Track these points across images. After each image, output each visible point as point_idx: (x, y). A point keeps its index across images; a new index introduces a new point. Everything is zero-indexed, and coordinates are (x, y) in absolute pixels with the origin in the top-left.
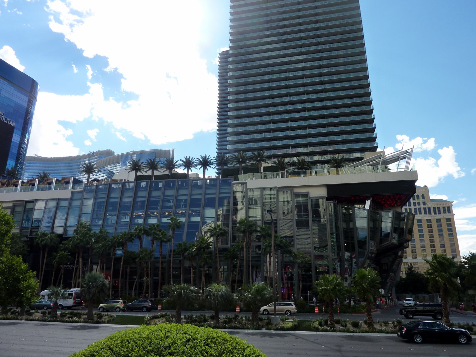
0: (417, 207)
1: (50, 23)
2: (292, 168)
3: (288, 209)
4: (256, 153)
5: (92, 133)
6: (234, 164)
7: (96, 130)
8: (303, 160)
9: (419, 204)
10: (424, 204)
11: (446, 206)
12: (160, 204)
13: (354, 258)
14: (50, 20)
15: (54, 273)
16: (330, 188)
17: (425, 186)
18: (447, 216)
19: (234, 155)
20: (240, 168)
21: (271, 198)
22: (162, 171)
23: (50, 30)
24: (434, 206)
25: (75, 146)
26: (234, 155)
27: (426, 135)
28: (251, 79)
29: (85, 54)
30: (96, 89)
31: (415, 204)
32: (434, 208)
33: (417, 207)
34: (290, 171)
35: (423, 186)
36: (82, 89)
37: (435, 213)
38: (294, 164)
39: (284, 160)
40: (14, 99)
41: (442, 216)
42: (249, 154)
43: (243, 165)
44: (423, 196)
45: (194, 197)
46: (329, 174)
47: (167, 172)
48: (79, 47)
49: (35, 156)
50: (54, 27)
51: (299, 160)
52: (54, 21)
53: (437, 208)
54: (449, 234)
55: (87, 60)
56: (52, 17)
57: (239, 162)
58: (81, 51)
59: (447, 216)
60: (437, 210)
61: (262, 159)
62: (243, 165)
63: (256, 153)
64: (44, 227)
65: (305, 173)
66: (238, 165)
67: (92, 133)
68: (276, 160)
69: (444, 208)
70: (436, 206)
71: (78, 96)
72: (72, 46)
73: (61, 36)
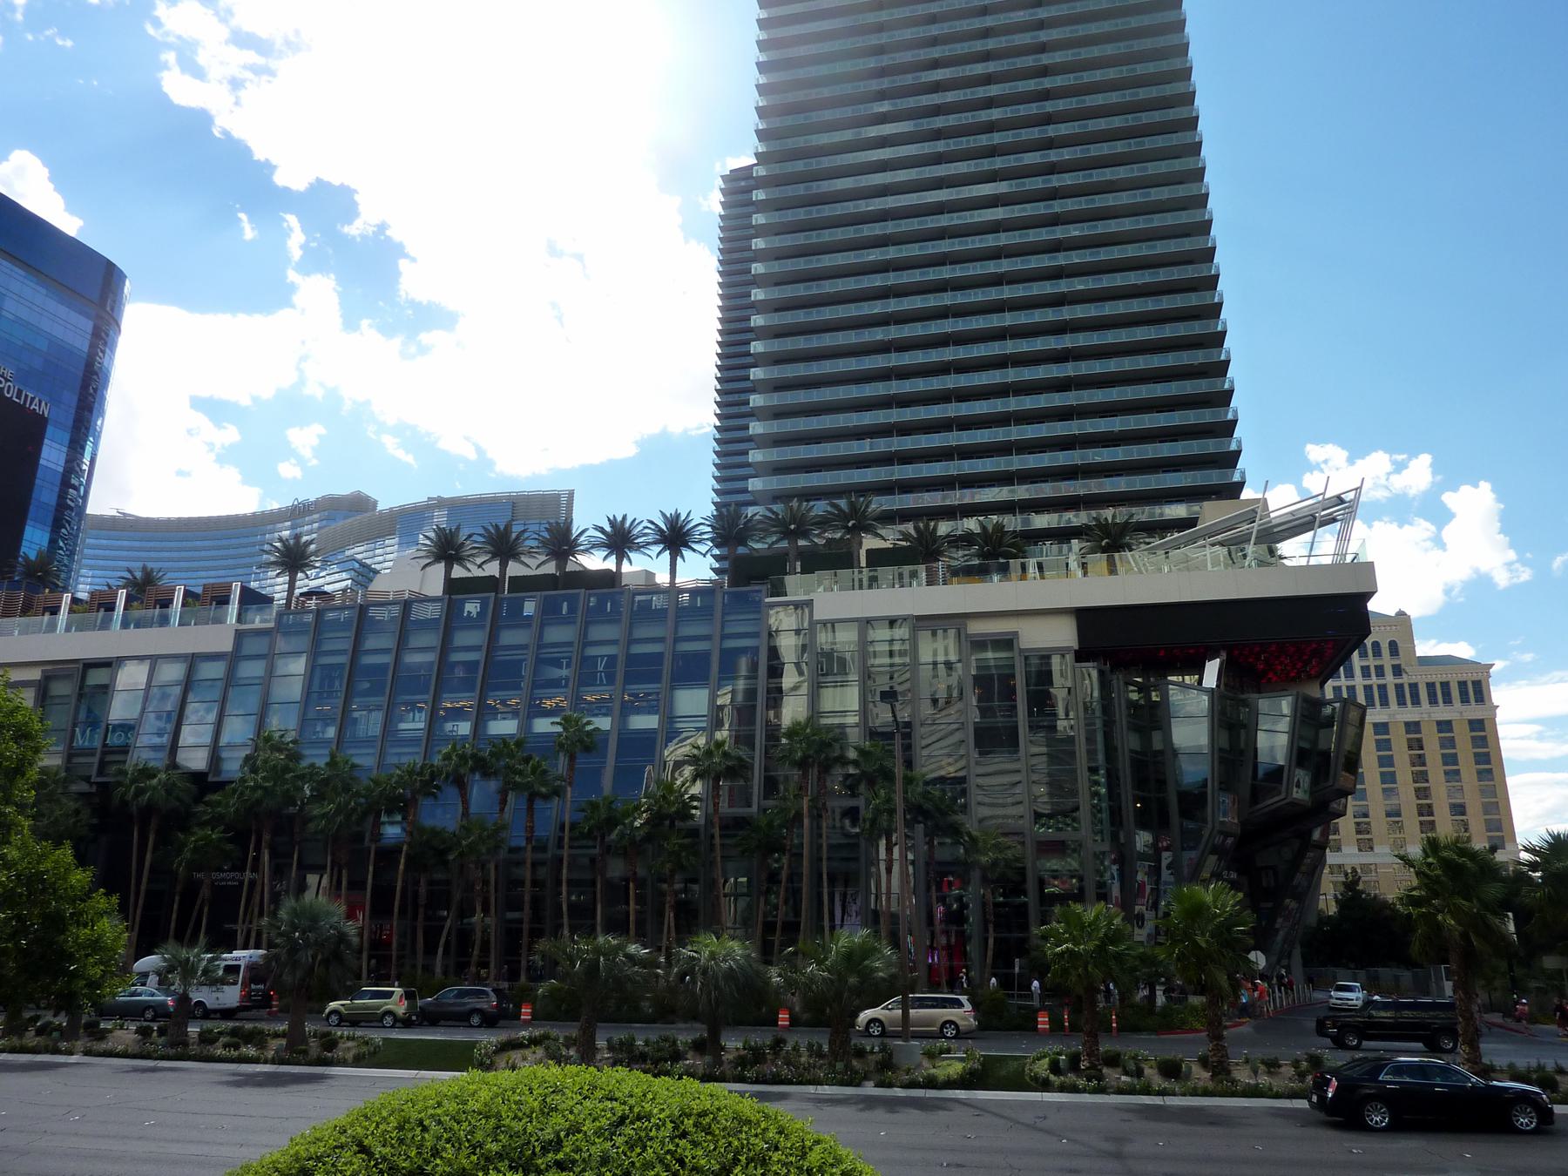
0: (1374, 680)
1: (165, 74)
2: (961, 553)
3: (949, 687)
4: (843, 503)
5: (304, 438)
6: (769, 540)
7: (317, 429)
8: (999, 527)
9: (1380, 671)
10: (1397, 670)
11: (1469, 677)
12: (526, 671)
13: (1167, 849)
14: (165, 66)
15: (177, 898)
16: (1086, 618)
17: (1401, 614)
18: (1474, 711)
19: (770, 510)
20: (792, 554)
21: (891, 654)
22: (534, 565)
23: (164, 100)
24: (1430, 680)
25: (248, 480)
26: (770, 510)
27: (1403, 445)
28: (828, 261)
29: (280, 179)
30: (318, 293)
31: (1366, 672)
32: (1431, 686)
33: (1374, 680)
34: (955, 563)
35: (1392, 614)
36: (269, 294)
37: (1433, 700)
38: (967, 539)
39: (935, 529)
40: (46, 325)
41: (1456, 712)
42: (820, 508)
43: (801, 543)
44: (1393, 646)
45: (638, 649)
46: (1085, 574)
47: (550, 568)
48: (259, 155)
49: (114, 513)
50: (179, 89)
51: (984, 528)
52: (176, 70)
53: (1438, 686)
54: (1479, 772)
55: (286, 199)
56: (170, 57)
57: (787, 534)
58: (268, 168)
59: (1474, 711)
60: (1440, 693)
61: (863, 524)
62: (801, 543)
63: (843, 503)
64: (146, 749)
65: (1004, 570)
66: (784, 544)
67: (304, 438)
68: (909, 527)
69: (1462, 685)
70: (1437, 679)
71: (258, 317)
72: (236, 151)
73: (201, 119)
